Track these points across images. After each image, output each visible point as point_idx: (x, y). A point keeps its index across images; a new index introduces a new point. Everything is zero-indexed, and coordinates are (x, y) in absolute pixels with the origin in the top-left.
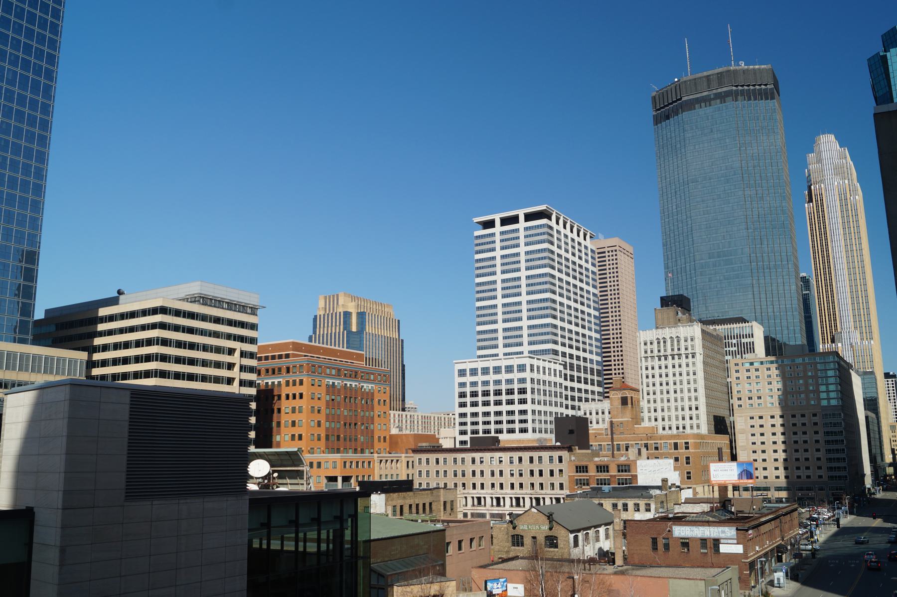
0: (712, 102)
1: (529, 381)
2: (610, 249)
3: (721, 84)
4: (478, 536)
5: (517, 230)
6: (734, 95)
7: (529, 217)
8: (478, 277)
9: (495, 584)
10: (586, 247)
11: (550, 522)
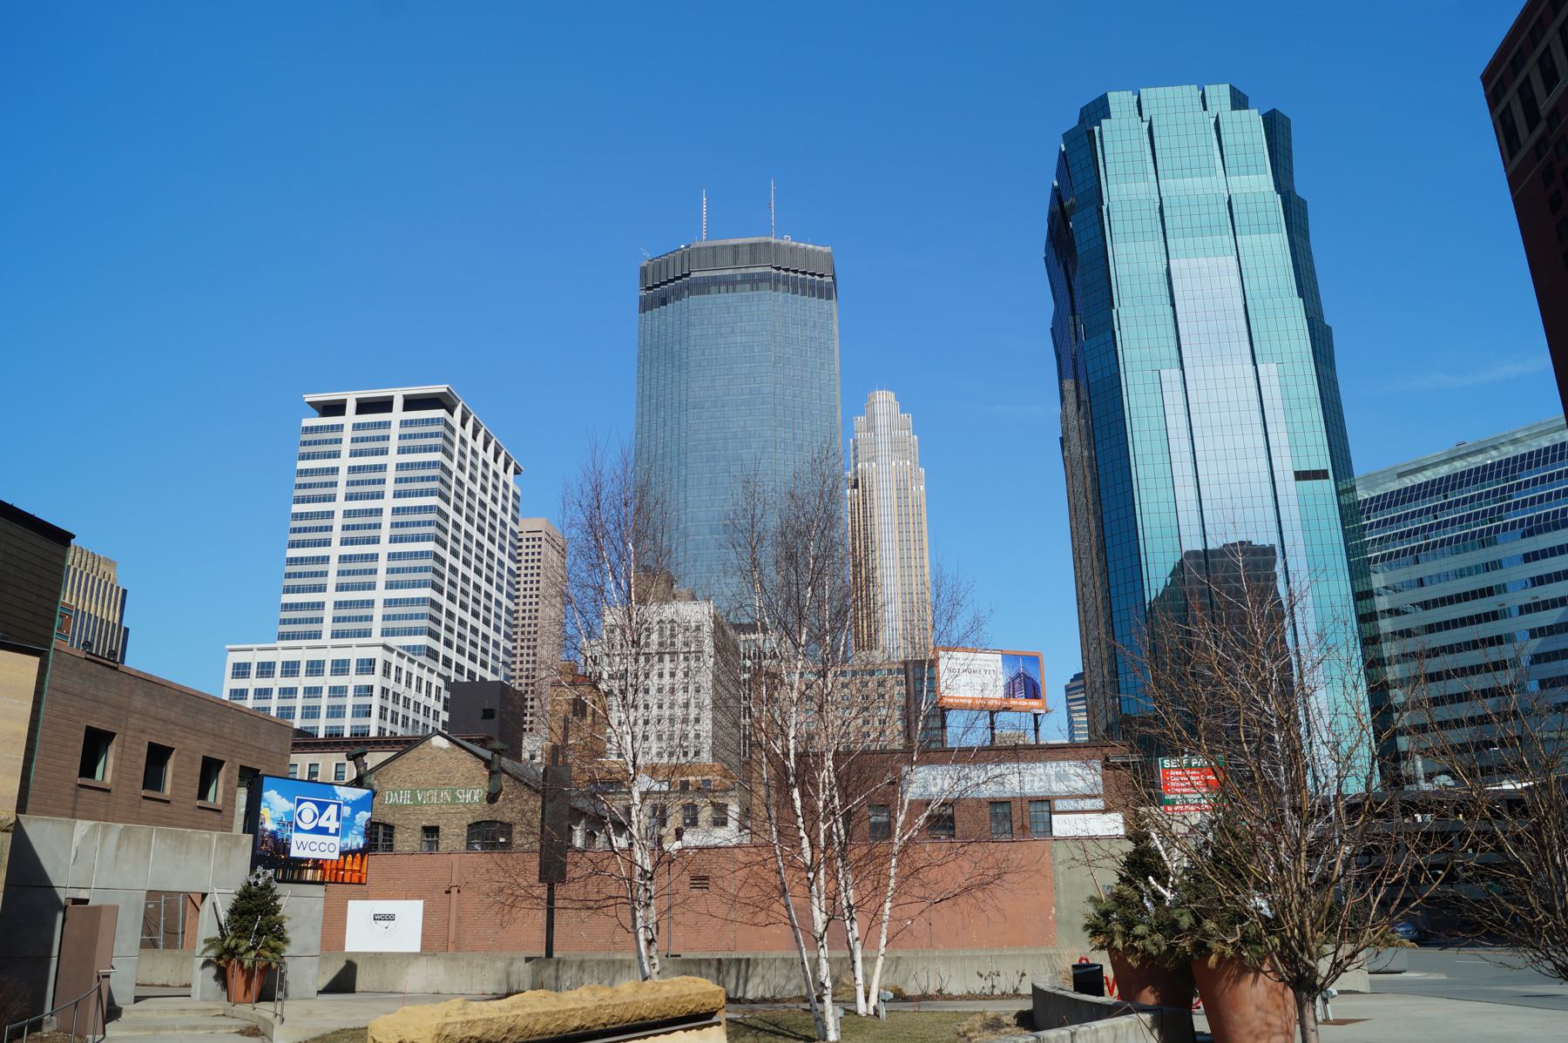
0: (738, 287)
1: (377, 691)
2: (530, 536)
3: (754, 262)
4: (239, 762)
5: (387, 425)
6: (775, 283)
7: (411, 403)
8: (288, 593)
9: (309, 809)
10: (506, 485)
11: (492, 773)
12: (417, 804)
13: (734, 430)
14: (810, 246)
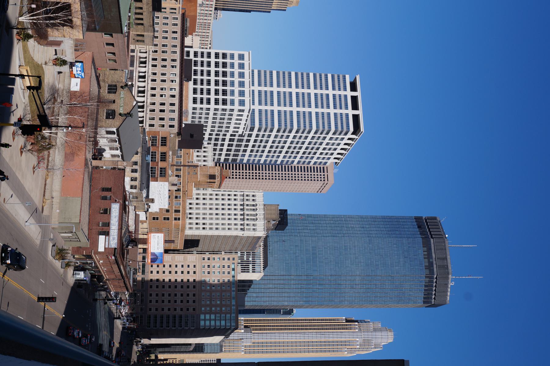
0: (427, 260)
1: (232, 107)
3: (439, 267)
5: (347, 108)
7: (356, 118)
8: (295, 74)
9: (80, 69)
12: (121, 98)
13: (359, 258)
14: (449, 294)
